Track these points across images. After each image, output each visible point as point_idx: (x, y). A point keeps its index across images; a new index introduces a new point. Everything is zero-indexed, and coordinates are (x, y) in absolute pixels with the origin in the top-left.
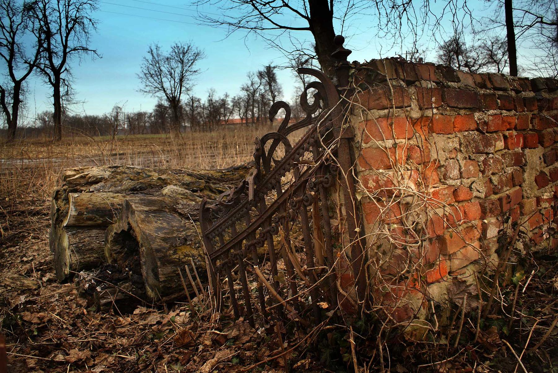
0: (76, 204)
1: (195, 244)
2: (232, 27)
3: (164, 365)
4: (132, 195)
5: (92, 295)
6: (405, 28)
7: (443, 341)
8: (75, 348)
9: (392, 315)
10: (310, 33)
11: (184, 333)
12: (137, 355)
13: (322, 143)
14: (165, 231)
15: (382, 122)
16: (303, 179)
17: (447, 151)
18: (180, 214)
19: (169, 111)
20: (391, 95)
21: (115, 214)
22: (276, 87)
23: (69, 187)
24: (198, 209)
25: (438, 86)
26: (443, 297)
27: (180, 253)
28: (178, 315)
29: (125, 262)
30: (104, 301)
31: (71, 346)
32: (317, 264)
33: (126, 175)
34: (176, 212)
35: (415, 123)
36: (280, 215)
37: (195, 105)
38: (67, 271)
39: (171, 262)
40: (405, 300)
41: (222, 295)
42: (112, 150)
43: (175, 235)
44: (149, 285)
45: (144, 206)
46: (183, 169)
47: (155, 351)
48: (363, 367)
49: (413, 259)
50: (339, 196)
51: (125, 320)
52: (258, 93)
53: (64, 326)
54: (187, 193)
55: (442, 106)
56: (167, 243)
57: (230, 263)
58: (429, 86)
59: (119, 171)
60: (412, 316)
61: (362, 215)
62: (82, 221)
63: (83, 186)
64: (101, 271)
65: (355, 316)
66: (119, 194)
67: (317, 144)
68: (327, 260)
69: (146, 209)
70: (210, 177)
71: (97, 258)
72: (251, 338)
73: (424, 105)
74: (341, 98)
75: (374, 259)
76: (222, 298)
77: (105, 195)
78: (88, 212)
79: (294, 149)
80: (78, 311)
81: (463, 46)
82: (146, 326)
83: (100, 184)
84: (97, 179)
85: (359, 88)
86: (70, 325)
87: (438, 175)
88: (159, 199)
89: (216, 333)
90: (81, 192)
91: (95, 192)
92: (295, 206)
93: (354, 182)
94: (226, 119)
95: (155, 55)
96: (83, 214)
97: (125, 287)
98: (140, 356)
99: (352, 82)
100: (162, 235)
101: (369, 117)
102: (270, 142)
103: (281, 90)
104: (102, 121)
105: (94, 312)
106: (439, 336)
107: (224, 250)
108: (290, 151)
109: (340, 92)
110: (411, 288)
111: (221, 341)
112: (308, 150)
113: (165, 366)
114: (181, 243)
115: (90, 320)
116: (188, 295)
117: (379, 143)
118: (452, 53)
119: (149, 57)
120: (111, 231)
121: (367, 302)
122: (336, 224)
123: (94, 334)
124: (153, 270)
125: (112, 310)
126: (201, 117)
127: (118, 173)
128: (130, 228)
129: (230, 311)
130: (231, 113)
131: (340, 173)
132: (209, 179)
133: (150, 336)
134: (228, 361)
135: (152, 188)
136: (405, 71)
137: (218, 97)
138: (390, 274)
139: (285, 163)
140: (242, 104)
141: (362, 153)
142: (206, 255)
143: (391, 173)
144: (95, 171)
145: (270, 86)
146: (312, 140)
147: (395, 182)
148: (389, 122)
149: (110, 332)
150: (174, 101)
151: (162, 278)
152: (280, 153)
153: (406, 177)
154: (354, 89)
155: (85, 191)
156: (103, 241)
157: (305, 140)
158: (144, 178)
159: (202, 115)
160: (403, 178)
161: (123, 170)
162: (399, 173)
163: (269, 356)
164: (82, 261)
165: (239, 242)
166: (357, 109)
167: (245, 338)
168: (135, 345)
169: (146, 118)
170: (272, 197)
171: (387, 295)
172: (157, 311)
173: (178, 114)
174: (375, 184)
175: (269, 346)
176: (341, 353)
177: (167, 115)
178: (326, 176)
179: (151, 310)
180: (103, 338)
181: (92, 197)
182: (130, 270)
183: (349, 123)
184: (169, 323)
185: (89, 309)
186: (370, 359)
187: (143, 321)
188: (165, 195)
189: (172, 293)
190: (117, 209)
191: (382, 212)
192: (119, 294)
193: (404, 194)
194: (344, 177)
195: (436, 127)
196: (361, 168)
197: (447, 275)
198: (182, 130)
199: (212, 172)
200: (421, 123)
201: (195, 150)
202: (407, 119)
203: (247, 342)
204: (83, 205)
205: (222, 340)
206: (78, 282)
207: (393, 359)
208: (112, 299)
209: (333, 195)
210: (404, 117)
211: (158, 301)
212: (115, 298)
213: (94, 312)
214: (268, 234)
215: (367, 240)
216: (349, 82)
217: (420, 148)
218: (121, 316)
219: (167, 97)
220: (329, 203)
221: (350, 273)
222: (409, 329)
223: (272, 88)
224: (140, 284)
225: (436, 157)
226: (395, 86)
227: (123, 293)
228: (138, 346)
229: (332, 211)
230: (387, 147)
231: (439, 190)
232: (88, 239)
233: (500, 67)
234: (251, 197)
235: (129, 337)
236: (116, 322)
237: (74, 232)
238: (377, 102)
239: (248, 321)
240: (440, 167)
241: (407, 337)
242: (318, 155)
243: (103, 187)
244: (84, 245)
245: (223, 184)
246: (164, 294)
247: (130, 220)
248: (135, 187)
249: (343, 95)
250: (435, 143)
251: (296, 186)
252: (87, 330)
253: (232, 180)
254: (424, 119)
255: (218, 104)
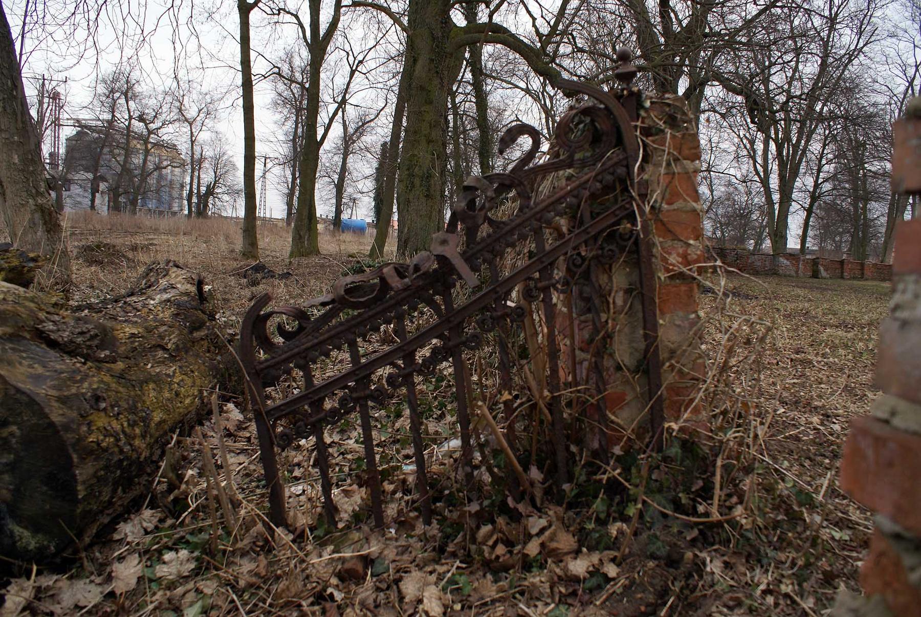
81: (136, 86)
118: (117, 95)
233: (194, 130)
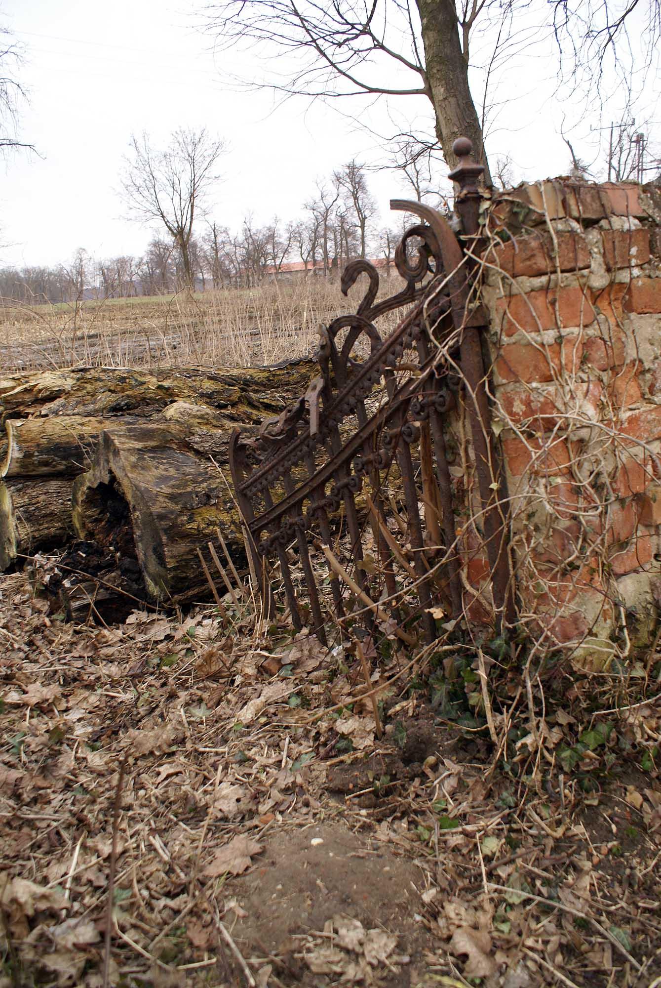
0: (19, 439)
1: (225, 503)
2: (280, 94)
3: (179, 707)
4: (113, 418)
5: (56, 594)
6: (610, 77)
7: (639, 672)
8: (35, 681)
9: (552, 629)
10: (425, 98)
11: (211, 655)
12: (136, 693)
13: (432, 338)
14: (172, 482)
15: (536, 298)
16: (401, 398)
17: (656, 344)
18: (197, 452)
19: (174, 253)
20: (553, 250)
21: (87, 452)
22: (366, 201)
23: (6, 409)
24: (227, 443)
25: (643, 226)
26: (642, 597)
27: (199, 519)
28: (199, 624)
29: (108, 536)
30: (77, 603)
31: (30, 678)
32: (428, 542)
33: (101, 384)
34: (191, 449)
35: (599, 296)
36: (365, 459)
37: (219, 240)
38: (13, 552)
39: (185, 536)
40: (573, 606)
41: (273, 590)
42: (75, 330)
43: (189, 490)
44: (150, 575)
45: (135, 440)
46: (200, 368)
47: (164, 685)
48: (502, 713)
49: (590, 536)
50: (464, 426)
51: (112, 634)
52: (335, 213)
53: (16, 646)
54: (207, 414)
55: (649, 262)
56: (176, 503)
57: (283, 538)
58: (626, 227)
59: (90, 377)
60: (587, 631)
61: (503, 460)
62: (31, 468)
63: (28, 406)
64: (69, 553)
65: (491, 630)
66: (91, 418)
67: (423, 336)
68: (444, 537)
69: (139, 445)
70: (248, 381)
71: (61, 528)
72: (321, 663)
73: (616, 263)
74: (464, 255)
75: (523, 536)
76: (272, 595)
77: (67, 421)
78: (41, 452)
79: (386, 345)
80: (36, 622)
82: (147, 644)
83: (58, 402)
84: (52, 392)
85: (496, 237)
86: (26, 644)
87: (639, 386)
88: (159, 427)
89: (263, 656)
90: (26, 417)
91: (51, 416)
92: (389, 443)
93: (488, 404)
94: (278, 263)
95: (142, 150)
96: (32, 455)
97: (111, 579)
98: (140, 695)
99: (484, 226)
100: (166, 490)
101: (515, 291)
102: (344, 331)
103: (375, 206)
104: (55, 275)
105: (62, 621)
106: (631, 666)
107: (272, 517)
108: (379, 347)
109: (463, 244)
110: (585, 585)
111: (271, 668)
112: (409, 346)
113: (182, 710)
114: (200, 502)
115: (56, 636)
116: (215, 592)
117: (531, 336)
119: (132, 154)
120: (82, 485)
121: (510, 607)
122: (460, 475)
123: (64, 658)
124: (155, 550)
125: (91, 618)
126: (232, 261)
127: (88, 381)
128: (113, 479)
129: (287, 617)
130: (286, 251)
131: (464, 388)
132: (246, 384)
133: (156, 661)
134: (283, 702)
135: (148, 404)
136: (582, 202)
137: (259, 226)
138: (549, 561)
139: (371, 368)
140: (306, 235)
141: (502, 352)
142: (243, 524)
143: (551, 389)
144: (47, 380)
145: (356, 198)
146: (416, 330)
147: (559, 405)
148: (550, 297)
149: (90, 654)
150: (181, 235)
151: (171, 563)
152: (362, 349)
153: (580, 394)
154: (488, 238)
155: (33, 414)
156: (69, 500)
157: (404, 330)
158: (133, 387)
159: (234, 258)
160: (572, 398)
161: (96, 375)
162: (567, 388)
163: (349, 694)
164: (36, 534)
165: (296, 503)
166: (494, 275)
167: (312, 664)
168: (131, 676)
169: (133, 267)
170: (349, 425)
171: (543, 597)
172: (164, 617)
173: (191, 258)
174: (524, 408)
175: (348, 678)
176: (466, 690)
177: (170, 261)
178: (441, 393)
179: (155, 616)
180: (79, 664)
181: (45, 426)
182: (117, 550)
183: (479, 299)
184: (184, 640)
185: (54, 617)
186: (513, 701)
187: (142, 635)
188: (170, 419)
189: (189, 588)
190: (89, 445)
191: (534, 457)
192: (101, 590)
193: (575, 425)
194: (471, 396)
195: (636, 301)
196: (500, 378)
197: (653, 560)
198: (198, 286)
199: (251, 372)
200: (609, 295)
201: (223, 325)
202: (583, 291)
203: (315, 669)
204: (32, 439)
205: (274, 667)
206: (32, 572)
207: (551, 703)
208: (89, 599)
209: (454, 424)
210: (578, 287)
211: (165, 602)
212: (94, 598)
213: (62, 621)
214: (346, 491)
215: (511, 502)
216: (478, 225)
217: (605, 342)
218: (106, 628)
219: (169, 227)
220: (447, 438)
221: (483, 558)
222: (579, 653)
223: (360, 202)
224: (135, 574)
225: (635, 356)
226: (562, 231)
227: (107, 589)
228: (136, 678)
229: (453, 453)
230: (545, 342)
231: (641, 414)
232: (43, 497)
234: (313, 428)
235: (121, 661)
236: (99, 637)
237: (20, 486)
238: (528, 263)
239: (315, 636)
240: (644, 372)
241: (577, 667)
242: (428, 354)
243: (63, 406)
244: (37, 508)
245: (272, 392)
246: (175, 590)
247: (114, 468)
248: (119, 404)
249: (468, 249)
250: (633, 332)
251: (390, 408)
252: (52, 653)
253: (287, 385)
254: (615, 287)
255: (261, 237)
